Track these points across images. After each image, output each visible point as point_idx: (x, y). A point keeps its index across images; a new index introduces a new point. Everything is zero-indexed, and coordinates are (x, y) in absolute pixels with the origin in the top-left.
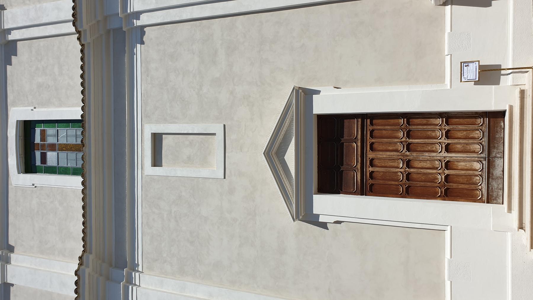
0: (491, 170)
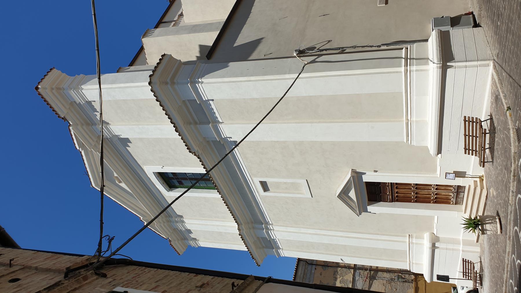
0: (458, 196)
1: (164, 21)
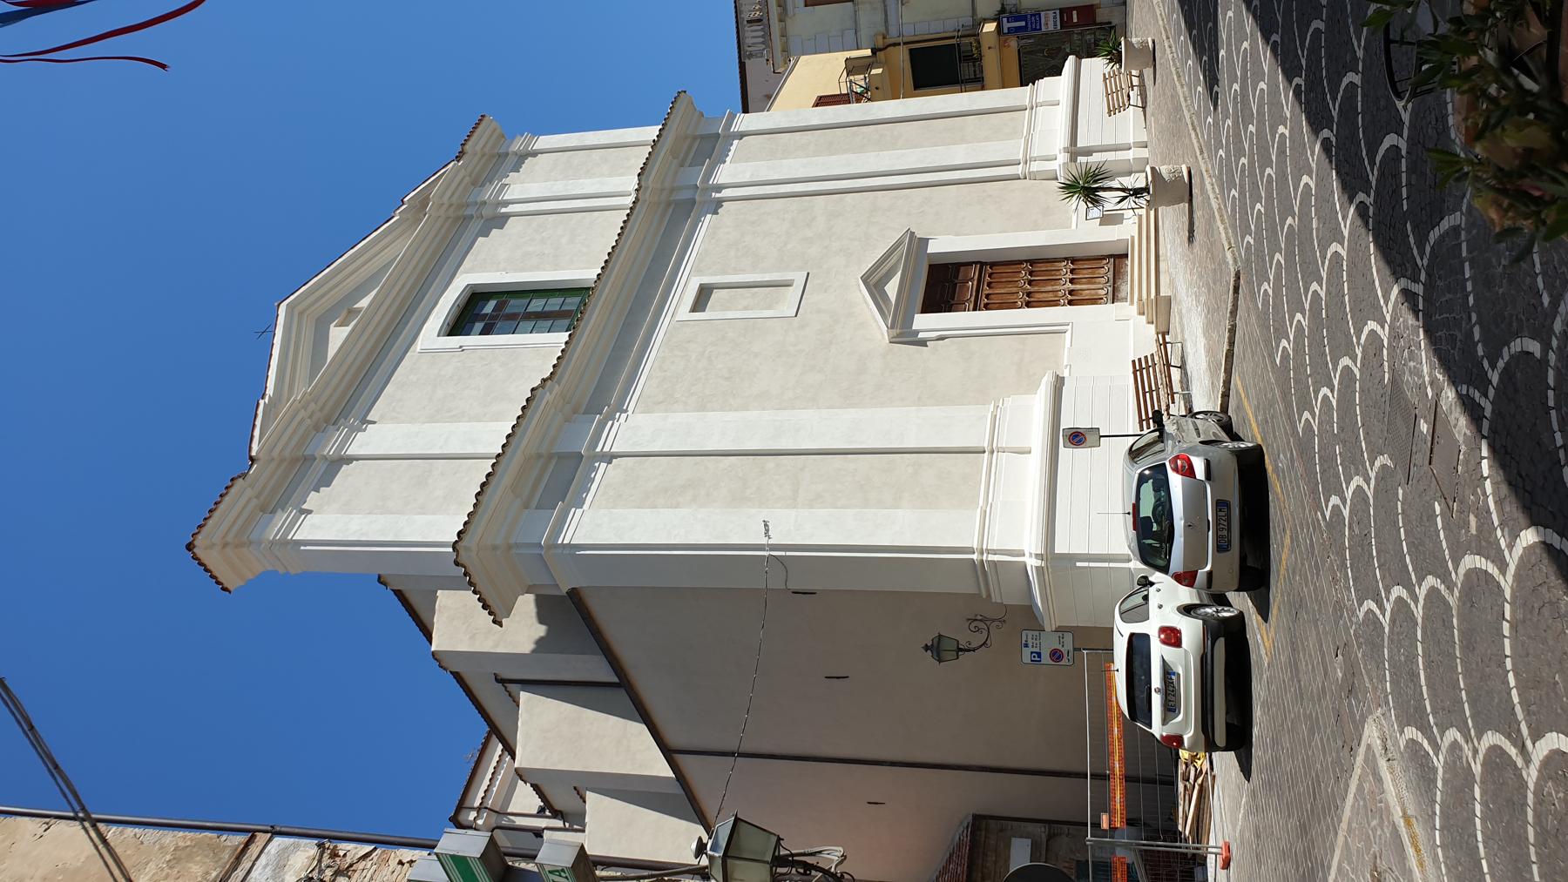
0: (1116, 294)
1: (506, 685)
